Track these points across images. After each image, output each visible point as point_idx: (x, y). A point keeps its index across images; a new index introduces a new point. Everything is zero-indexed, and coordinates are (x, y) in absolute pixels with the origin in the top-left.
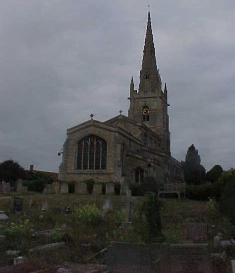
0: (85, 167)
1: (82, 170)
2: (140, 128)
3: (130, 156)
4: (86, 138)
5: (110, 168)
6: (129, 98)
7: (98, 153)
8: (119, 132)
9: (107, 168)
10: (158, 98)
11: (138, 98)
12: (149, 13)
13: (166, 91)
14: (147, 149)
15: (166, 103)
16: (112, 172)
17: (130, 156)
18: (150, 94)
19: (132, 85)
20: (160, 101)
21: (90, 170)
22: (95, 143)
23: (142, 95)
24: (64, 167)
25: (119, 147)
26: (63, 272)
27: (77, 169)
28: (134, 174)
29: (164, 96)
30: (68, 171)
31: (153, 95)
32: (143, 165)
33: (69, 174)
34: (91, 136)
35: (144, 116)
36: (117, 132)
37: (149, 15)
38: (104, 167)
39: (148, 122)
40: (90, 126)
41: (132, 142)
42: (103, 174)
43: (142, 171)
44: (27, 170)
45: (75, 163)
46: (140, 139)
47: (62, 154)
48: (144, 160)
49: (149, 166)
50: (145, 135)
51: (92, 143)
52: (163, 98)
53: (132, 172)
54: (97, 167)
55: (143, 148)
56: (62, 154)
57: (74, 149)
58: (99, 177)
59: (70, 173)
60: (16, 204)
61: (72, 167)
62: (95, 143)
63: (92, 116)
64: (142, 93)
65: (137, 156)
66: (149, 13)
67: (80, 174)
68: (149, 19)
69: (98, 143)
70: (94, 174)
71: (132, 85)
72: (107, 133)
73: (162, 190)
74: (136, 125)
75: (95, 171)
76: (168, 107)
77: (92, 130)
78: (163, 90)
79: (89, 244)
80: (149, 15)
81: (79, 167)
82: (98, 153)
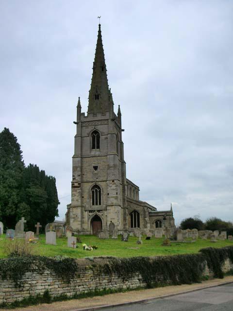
0: (97, 204)
6: (75, 123)
12: (100, 25)
13: (119, 114)
15: (120, 128)
18: (99, 117)
19: (79, 107)
20: (111, 124)
23: (91, 118)
26: (46, 298)
28: (155, 224)
29: (117, 120)
31: (103, 118)
37: (100, 28)
39: (98, 149)
44: (23, 163)
60: (20, 171)
64: (92, 115)
66: (100, 25)
68: (100, 32)
71: (79, 107)
76: (122, 132)
78: (116, 112)
79: (71, 294)
80: (100, 28)
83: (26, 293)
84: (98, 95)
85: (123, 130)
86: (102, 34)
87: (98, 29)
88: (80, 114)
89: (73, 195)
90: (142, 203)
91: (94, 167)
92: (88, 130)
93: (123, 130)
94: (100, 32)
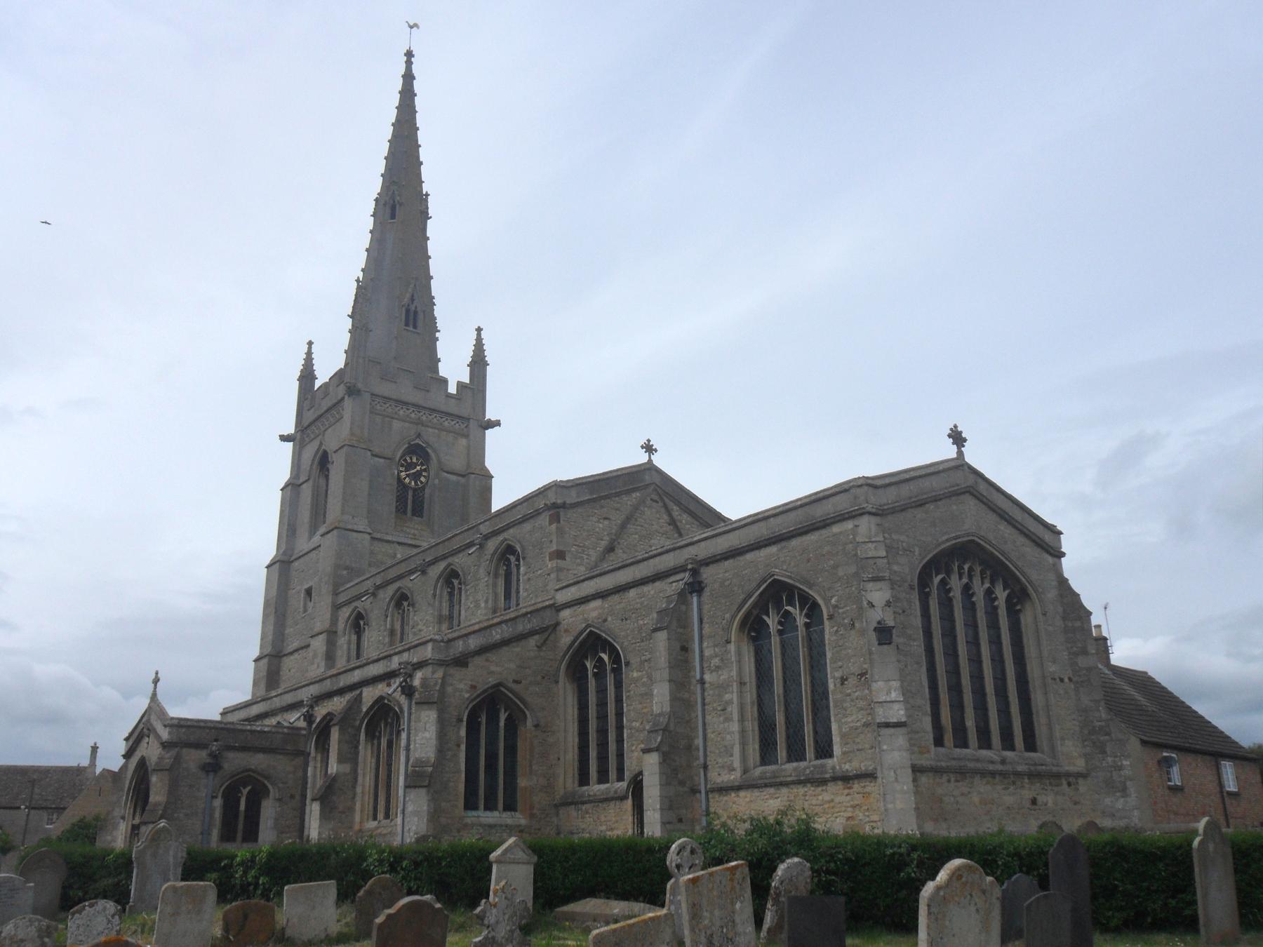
12: (409, 54)
66: (409, 54)
68: (409, 78)
94: (409, 78)
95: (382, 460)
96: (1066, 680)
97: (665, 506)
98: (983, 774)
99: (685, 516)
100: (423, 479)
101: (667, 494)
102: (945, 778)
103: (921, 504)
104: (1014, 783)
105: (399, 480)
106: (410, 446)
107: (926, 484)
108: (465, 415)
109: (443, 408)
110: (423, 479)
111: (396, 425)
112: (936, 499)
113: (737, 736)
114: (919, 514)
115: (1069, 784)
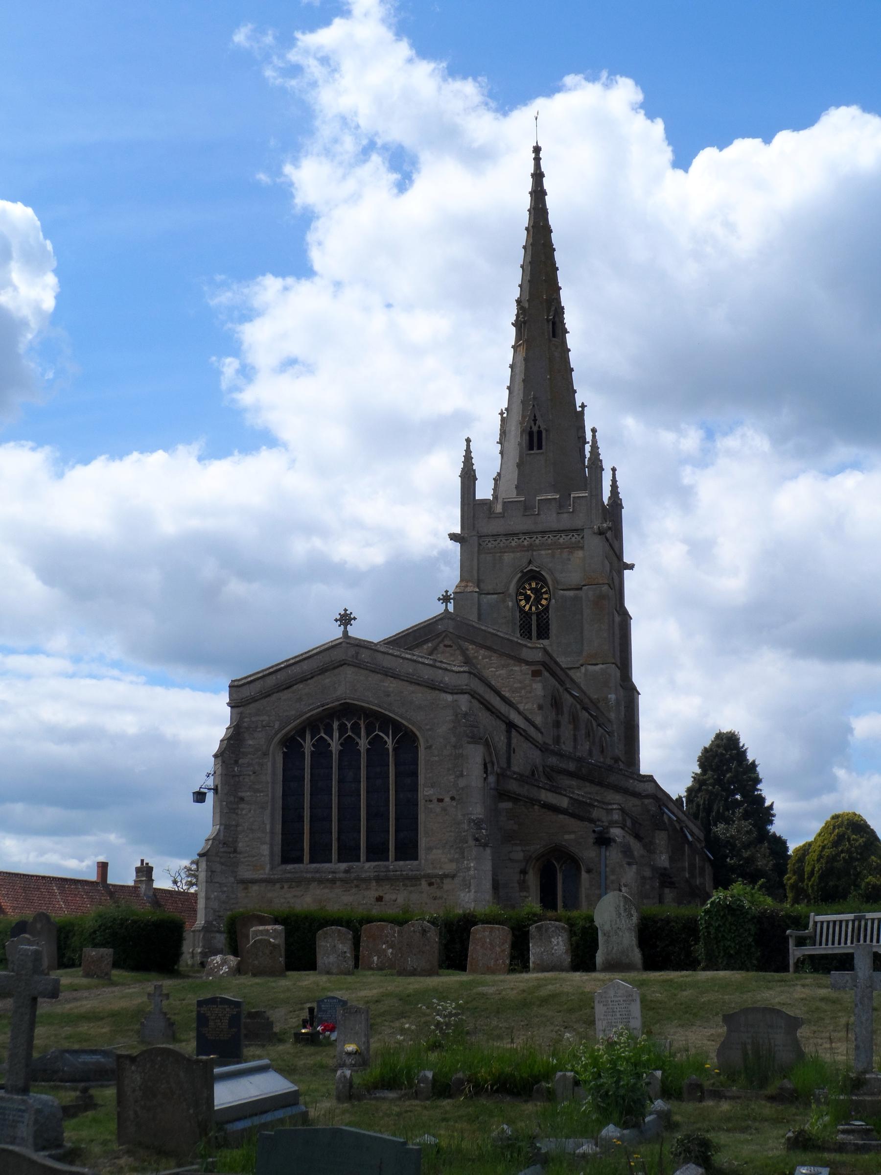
0: (320, 854)
1: (307, 867)
2: (536, 674)
3: (515, 799)
4: (317, 724)
5: (435, 851)
7: (377, 789)
8: (473, 695)
9: (422, 853)
10: (587, 533)
11: (495, 536)
12: (537, 150)
14: (572, 766)
15: (619, 555)
16: (450, 868)
17: (515, 799)
19: (468, 476)
21: (343, 866)
22: (363, 744)
24: (219, 856)
25: (475, 756)
27: (285, 860)
28: (533, 880)
30: (246, 873)
32: (574, 835)
33: (246, 883)
34: (347, 710)
35: (526, 616)
36: (463, 692)
37: (537, 160)
38: (408, 849)
40: (343, 664)
41: (514, 733)
42: (413, 880)
43: (573, 863)
45: (272, 832)
46: (538, 720)
47: (210, 796)
48: (580, 812)
49: (603, 841)
50: (556, 703)
51: (349, 745)
52: (609, 534)
53: (524, 872)
54: (377, 852)
55: (553, 760)
56: (210, 796)
57: (270, 771)
58: (387, 897)
59: (253, 882)
61: (261, 849)
62: (363, 744)
63: (345, 619)
65: (546, 796)
66: (537, 150)
67: (298, 882)
68: (538, 176)
69: (376, 744)
70: (362, 882)
72: (420, 696)
73: (801, 942)
74: (521, 661)
75: (367, 867)
77: (345, 687)
80: (537, 160)
81: (290, 853)
82: (377, 789)
83: (417, 1105)
84: (540, 433)
85: (631, 567)
86: (547, 184)
87: (532, 163)
88: (470, 505)
89: (215, 765)
90: (644, 776)
91: (403, 185)
92: (512, 561)
93: (631, 567)
94: (538, 176)
95: (496, 596)
96: (447, 799)
97: (460, 648)
98: (321, 881)
99: (482, 652)
100: (544, 602)
101: (459, 637)
102: (278, 886)
103: (288, 686)
104: (357, 886)
105: (521, 610)
106: (524, 574)
107: (296, 669)
108: (580, 527)
109: (555, 526)
110: (544, 602)
111: (508, 557)
112: (304, 680)
113: (267, 859)
114: (285, 695)
115: (431, 884)
